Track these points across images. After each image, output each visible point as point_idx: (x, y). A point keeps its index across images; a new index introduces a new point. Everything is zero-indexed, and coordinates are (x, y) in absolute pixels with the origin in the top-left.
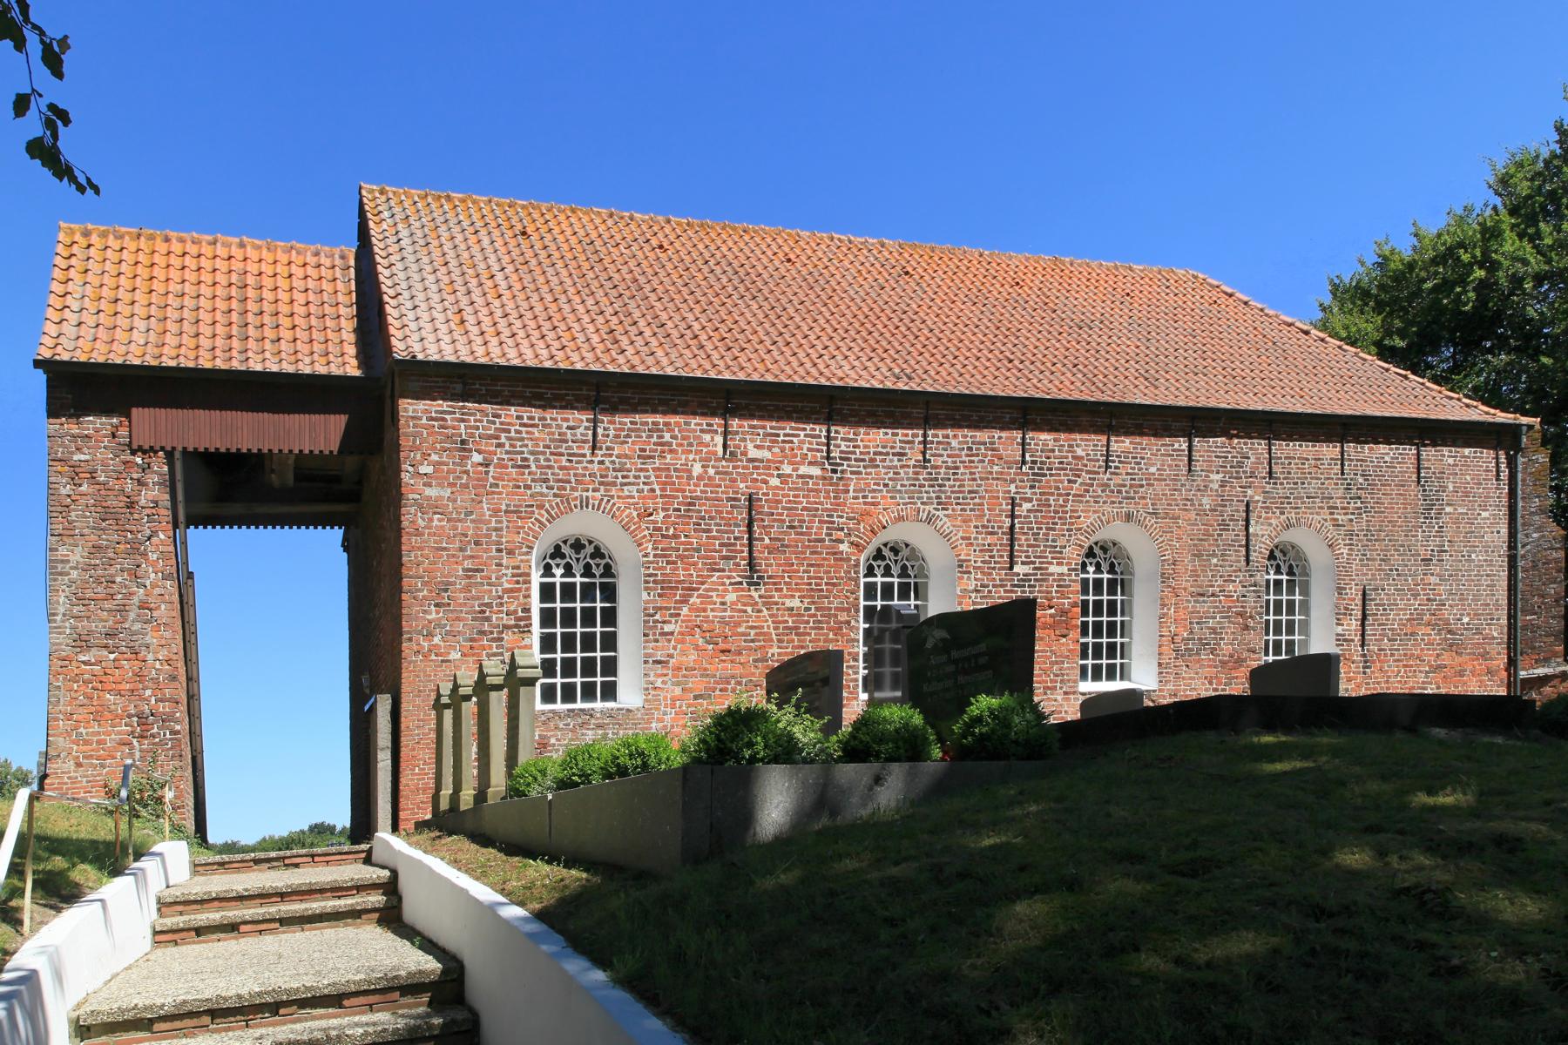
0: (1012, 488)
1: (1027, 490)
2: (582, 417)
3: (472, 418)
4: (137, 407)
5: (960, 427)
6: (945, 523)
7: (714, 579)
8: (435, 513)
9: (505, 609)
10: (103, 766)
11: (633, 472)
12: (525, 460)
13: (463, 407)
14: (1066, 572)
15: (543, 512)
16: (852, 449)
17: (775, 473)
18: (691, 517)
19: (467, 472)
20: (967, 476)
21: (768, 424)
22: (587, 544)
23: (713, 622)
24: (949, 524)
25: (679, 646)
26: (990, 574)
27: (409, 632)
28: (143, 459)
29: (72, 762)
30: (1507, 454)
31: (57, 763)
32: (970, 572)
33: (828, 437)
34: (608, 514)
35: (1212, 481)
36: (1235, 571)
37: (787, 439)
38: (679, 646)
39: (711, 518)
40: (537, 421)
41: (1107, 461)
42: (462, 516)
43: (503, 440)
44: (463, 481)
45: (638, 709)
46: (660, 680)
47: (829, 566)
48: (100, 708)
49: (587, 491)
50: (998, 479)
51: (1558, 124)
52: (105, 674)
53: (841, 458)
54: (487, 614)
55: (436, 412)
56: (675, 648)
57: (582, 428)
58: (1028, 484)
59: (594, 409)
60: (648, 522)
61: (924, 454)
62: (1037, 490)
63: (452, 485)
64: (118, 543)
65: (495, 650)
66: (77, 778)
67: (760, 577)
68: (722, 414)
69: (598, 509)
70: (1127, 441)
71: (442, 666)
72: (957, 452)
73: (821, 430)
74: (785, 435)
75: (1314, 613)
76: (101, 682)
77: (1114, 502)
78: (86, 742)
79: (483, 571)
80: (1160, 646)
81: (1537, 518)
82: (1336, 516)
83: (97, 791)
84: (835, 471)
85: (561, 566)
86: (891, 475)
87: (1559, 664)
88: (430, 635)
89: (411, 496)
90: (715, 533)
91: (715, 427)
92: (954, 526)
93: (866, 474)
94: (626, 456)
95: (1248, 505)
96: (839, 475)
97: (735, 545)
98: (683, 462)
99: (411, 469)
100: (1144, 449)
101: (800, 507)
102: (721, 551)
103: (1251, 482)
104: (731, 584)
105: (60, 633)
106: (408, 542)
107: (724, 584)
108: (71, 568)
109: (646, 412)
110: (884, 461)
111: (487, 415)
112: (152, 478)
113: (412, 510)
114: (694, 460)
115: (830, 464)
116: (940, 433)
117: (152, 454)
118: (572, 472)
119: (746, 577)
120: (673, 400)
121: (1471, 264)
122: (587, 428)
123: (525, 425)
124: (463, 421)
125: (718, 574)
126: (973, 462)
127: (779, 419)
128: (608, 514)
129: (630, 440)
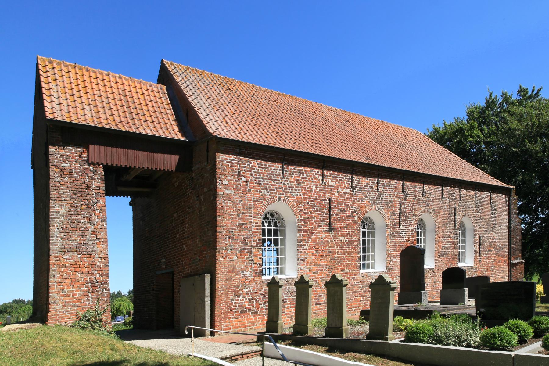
0: (400, 200)
1: (404, 201)
2: (278, 166)
3: (242, 163)
4: (92, 144)
5: (387, 179)
6: (383, 211)
7: (319, 229)
8: (229, 200)
9: (253, 240)
10: (75, 306)
11: (294, 188)
12: (260, 181)
13: (239, 158)
14: (413, 229)
15: (266, 202)
16: (358, 184)
17: (337, 191)
18: (312, 206)
19: (240, 184)
20: (389, 196)
21: (335, 173)
22: (275, 214)
23: (319, 245)
24: (384, 212)
25: (308, 254)
26: (394, 229)
27: (219, 249)
28: (93, 168)
29: (61, 305)
30: (508, 196)
31: (54, 306)
32: (389, 229)
33: (352, 179)
34: (287, 203)
35: (447, 201)
36: (452, 230)
37: (340, 179)
38: (308, 254)
39: (318, 207)
40: (264, 166)
41: (423, 193)
42: (238, 202)
43: (252, 173)
44: (239, 188)
45: (296, 278)
46: (302, 267)
47: (352, 225)
48: (74, 280)
49: (280, 194)
50: (396, 197)
51: (49, 61)
52: (76, 264)
53: (355, 187)
54: (246, 241)
55: (230, 159)
56: (307, 255)
57: (279, 170)
58: (404, 199)
59: (282, 163)
60: (299, 207)
61: (377, 187)
62: (406, 201)
63: (235, 189)
64: (82, 205)
65: (249, 256)
66: (63, 312)
67: (332, 229)
68: (322, 168)
69: (284, 202)
70: (428, 186)
71: (231, 262)
72: (386, 187)
73: (350, 176)
74: (340, 178)
75: (467, 243)
76: (74, 268)
77: (424, 206)
78: (68, 295)
79: (245, 224)
80: (435, 254)
81: (514, 216)
82: (474, 213)
83: (72, 318)
84: (353, 191)
85: (267, 223)
86: (369, 194)
87: (520, 260)
88: (227, 250)
89: (220, 193)
90: (319, 212)
91: (320, 173)
92: (385, 212)
93: (362, 193)
94: (292, 182)
95: (455, 209)
96: (355, 193)
97: (325, 217)
98: (310, 185)
99: (220, 182)
100: (431, 189)
101: (344, 204)
102: (320, 219)
103: (456, 202)
104: (324, 231)
105: (55, 245)
106: (219, 212)
107: (322, 231)
108: (60, 215)
109: (298, 165)
110: (367, 189)
111: (247, 163)
112: (97, 177)
113: (221, 198)
114: (313, 185)
115: (352, 189)
116: (382, 180)
117: (97, 166)
118: (275, 187)
119: (328, 229)
120: (308, 162)
121: (468, 136)
122: (280, 170)
123: (260, 167)
124: (239, 164)
125: (320, 227)
126: (390, 191)
127: (338, 172)
128: (287, 203)
129: (294, 176)
